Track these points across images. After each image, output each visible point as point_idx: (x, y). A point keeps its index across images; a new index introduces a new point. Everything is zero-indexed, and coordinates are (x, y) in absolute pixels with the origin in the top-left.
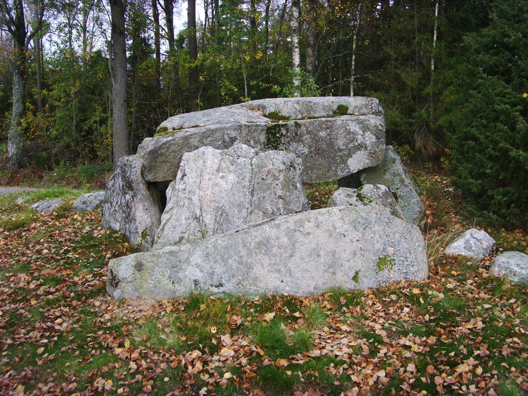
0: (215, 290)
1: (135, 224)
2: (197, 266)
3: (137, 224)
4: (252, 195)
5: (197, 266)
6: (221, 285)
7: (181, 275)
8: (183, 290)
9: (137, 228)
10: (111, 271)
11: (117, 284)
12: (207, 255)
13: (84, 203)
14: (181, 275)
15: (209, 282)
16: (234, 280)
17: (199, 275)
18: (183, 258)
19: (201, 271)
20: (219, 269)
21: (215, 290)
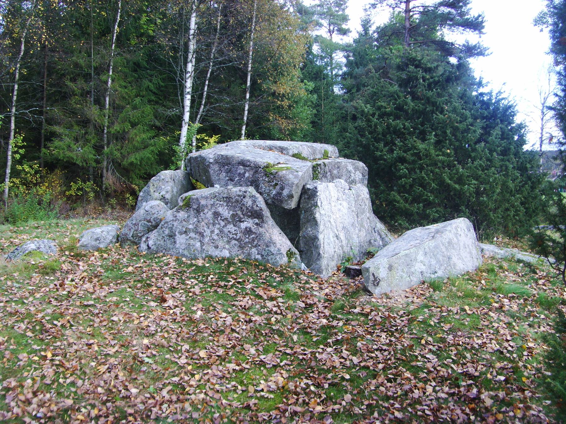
0: (433, 276)
1: (275, 247)
2: (421, 262)
3: (278, 246)
4: (358, 217)
5: (421, 262)
6: (436, 272)
7: (413, 270)
8: (415, 280)
9: (279, 250)
10: (373, 274)
11: (378, 284)
12: (426, 254)
13: (97, 239)
14: (413, 270)
15: (429, 271)
16: (443, 268)
17: (423, 268)
18: (413, 258)
19: (424, 265)
20: (433, 262)
21: (433, 276)
